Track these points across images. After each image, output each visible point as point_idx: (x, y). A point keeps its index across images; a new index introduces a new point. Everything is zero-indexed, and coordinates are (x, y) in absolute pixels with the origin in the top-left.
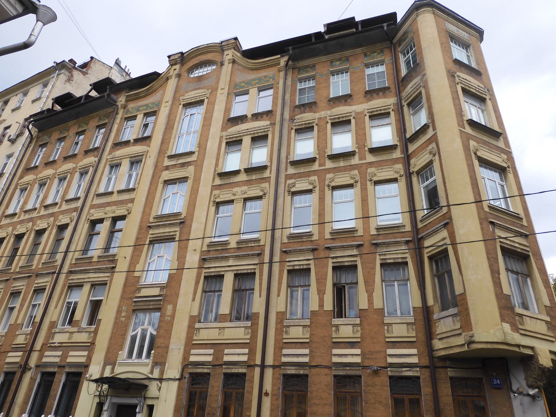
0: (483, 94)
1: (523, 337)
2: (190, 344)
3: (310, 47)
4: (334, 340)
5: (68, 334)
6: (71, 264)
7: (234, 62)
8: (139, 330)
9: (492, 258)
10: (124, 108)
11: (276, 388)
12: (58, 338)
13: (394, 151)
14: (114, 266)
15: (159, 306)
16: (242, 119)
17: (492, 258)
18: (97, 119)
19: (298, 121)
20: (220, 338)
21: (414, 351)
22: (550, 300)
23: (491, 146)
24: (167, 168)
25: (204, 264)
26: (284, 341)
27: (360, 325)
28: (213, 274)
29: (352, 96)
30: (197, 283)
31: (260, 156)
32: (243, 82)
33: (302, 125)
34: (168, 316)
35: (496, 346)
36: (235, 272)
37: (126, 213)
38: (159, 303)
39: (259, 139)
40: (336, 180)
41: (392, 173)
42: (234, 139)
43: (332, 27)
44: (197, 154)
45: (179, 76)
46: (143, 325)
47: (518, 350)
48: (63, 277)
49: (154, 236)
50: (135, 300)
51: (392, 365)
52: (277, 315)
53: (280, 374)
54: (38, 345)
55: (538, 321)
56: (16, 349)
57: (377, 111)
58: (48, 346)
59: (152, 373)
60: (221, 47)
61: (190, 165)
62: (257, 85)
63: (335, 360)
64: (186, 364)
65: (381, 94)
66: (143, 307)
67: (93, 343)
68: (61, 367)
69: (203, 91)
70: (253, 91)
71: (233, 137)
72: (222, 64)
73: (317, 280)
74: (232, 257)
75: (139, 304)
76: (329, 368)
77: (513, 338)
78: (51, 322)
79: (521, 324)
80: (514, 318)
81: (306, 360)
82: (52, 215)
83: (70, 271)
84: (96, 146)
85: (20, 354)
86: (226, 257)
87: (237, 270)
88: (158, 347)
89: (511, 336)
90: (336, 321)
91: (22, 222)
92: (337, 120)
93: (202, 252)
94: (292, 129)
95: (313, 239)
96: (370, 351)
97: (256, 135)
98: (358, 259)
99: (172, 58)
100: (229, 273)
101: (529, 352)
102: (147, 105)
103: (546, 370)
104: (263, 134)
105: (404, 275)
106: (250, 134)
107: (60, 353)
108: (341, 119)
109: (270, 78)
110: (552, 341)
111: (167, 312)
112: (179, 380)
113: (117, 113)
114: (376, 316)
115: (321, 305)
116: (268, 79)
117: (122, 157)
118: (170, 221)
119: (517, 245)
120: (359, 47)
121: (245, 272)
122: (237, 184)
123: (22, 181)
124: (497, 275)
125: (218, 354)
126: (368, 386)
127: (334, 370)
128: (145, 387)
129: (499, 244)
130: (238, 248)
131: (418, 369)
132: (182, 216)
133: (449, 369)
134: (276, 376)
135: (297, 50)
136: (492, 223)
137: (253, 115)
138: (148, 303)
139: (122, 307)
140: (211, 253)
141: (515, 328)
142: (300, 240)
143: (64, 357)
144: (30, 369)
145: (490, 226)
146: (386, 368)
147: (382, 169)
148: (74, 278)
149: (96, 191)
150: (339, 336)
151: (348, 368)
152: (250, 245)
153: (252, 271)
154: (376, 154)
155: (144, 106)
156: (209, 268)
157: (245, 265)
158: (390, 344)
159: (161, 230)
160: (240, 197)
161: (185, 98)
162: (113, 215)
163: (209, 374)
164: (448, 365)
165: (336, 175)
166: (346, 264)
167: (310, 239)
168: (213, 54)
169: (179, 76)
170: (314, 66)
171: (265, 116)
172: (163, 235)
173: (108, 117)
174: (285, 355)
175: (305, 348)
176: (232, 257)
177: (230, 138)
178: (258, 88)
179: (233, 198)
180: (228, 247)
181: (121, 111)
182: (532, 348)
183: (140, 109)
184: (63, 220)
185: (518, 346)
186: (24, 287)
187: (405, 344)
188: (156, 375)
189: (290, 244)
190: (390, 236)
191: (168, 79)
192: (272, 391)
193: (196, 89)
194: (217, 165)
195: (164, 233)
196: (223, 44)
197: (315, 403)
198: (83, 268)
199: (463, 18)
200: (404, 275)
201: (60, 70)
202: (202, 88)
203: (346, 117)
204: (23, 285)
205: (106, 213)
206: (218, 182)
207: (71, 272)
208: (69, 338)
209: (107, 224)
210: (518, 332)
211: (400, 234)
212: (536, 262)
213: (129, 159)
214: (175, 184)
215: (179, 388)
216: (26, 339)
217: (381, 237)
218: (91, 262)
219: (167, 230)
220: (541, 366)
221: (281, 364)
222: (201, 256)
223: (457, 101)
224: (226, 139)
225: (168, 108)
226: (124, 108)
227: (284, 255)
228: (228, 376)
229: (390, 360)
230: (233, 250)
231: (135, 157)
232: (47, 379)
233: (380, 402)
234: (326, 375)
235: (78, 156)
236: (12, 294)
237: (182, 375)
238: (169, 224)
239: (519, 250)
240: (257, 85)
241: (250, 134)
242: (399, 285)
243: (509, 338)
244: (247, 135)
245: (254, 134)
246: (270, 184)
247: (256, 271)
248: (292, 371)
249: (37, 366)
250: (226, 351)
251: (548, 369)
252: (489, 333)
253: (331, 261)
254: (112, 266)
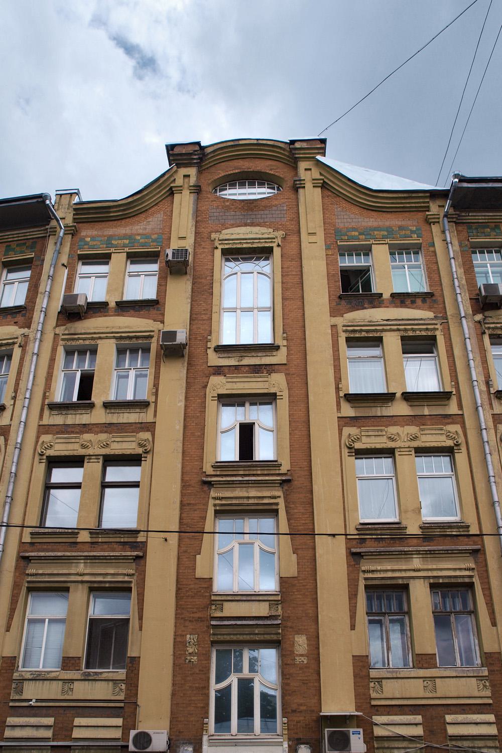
4: (374, 703)
8: (233, 680)
13: (390, 404)
14: (141, 554)
16: (97, 308)
21: (491, 718)
24: (219, 371)
25: (26, 568)
28: (107, 585)
30: (353, 596)
31: (422, 375)
32: (354, 229)
34: (302, 655)
38: (273, 630)
39: (418, 344)
41: (443, 438)
42: (364, 334)
44: (284, 350)
46: (239, 670)
49: (224, 502)
61: (274, 371)
62: (388, 241)
66: (228, 638)
69: (264, 230)
70: (118, 258)
71: (361, 331)
72: (297, 187)
74: (86, 558)
75: (218, 631)
86: (406, 553)
88: (294, 711)
94: (484, 333)
97: (411, 334)
98: (475, 573)
100: (417, 581)
102: (129, 237)
104: (424, 333)
105: (465, 604)
106: (398, 330)
109: (412, 232)
111: (297, 647)
116: (408, 232)
118: (254, 475)
122: (393, 420)
125: (63, 729)
130: (92, 543)
132: (283, 469)
137: (393, 295)
138: (247, 630)
139: (184, 636)
149: (45, 397)
150: (383, 696)
154: (357, 405)
155: (125, 237)
157: (451, 568)
159: (239, 492)
160: (407, 444)
161: (222, 237)
168: (270, 162)
169: (197, 190)
171: (419, 301)
172: (245, 501)
173: (32, 247)
174: (47, 727)
175: (118, 717)
176: (418, 552)
178: (128, 253)
179: (82, 452)
183: (386, 233)
191: (171, 193)
194: (338, 379)
195: (248, 498)
196: (297, 145)
198: (59, 554)
200: (465, 604)
202: (258, 225)
203: (376, 331)
206: (348, 411)
213: (113, 341)
214: (243, 405)
218: (76, 543)
219: (253, 493)
222: (19, 552)
230: (415, 541)
231: (130, 338)
238: (256, 482)
240: (127, 250)
241: (398, 330)
244: (107, 338)
245: (406, 330)
246: (6, 440)
247: (474, 580)
250: (78, 721)
253: (362, 575)
254: (135, 553)
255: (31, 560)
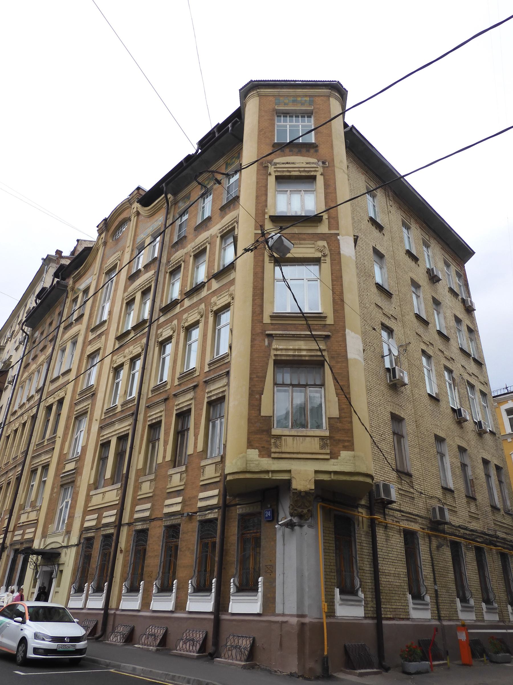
0: (311, 171)
1: (276, 461)
2: (86, 512)
3: (180, 176)
5: (179, 475)
6: (148, 399)
7: (138, 214)
10: (73, 290)
11: (129, 544)
12: (24, 518)
15: (72, 480)
17: (257, 377)
18: (59, 307)
19: (172, 262)
20: (103, 502)
23: (304, 236)
26: (138, 498)
27: (186, 471)
29: (317, 146)
33: (174, 265)
36: (118, 436)
37: (229, 300)
40: (189, 319)
43: (202, 143)
45: (105, 243)
47: (267, 477)
48: (141, 417)
50: (61, 476)
51: (202, 509)
53: (132, 531)
54: (11, 528)
56: (206, 487)
57: (226, 228)
58: (136, 502)
59: (63, 542)
60: (129, 202)
63: (166, 510)
64: (84, 530)
65: (232, 206)
67: (37, 520)
68: (22, 543)
73: (165, 430)
76: (160, 519)
77: (259, 464)
78: (20, 505)
79: (276, 447)
80: (269, 442)
81: (147, 514)
82: (201, 301)
83: (101, 427)
84: (206, 216)
85: (216, 492)
87: (119, 433)
89: (257, 463)
90: (171, 471)
91: (22, 414)
92: (198, 251)
93: (101, 420)
95: (167, 389)
96: (189, 498)
97: (144, 288)
99: (100, 227)
101: (285, 477)
107: (149, 506)
108: (201, 249)
112: (77, 545)
113: (67, 297)
114: (197, 460)
115: (164, 457)
117: (66, 342)
120: (219, 159)
121: (123, 434)
123: (23, 379)
124: (257, 396)
126: (184, 533)
127: (165, 521)
128: (59, 554)
129: (274, 358)
131: (217, 510)
132: (197, 373)
133: (238, 506)
134: (130, 533)
135: (171, 184)
136: (270, 336)
140: (107, 420)
142: (159, 392)
143: (99, 519)
144: (7, 548)
146: (196, 513)
147: (221, 295)
148: (212, 389)
151: (172, 518)
152: (129, 406)
153: (220, 395)
156: (103, 436)
158: (203, 487)
162: (131, 356)
163: (93, 537)
164: (237, 502)
165: (189, 314)
166: (185, 409)
167: (165, 389)
170: (190, 193)
177: (143, 287)
180: (116, 412)
181: (70, 294)
182: (289, 471)
184: (118, 361)
185: (267, 472)
186: (163, 413)
187: (212, 485)
188: (64, 544)
189: (153, 398)
190: (218, 369)
192: (126, 549)
193: (114, 253)
197: (149, 556)
199: (303, 81)
201: (48, 265)
204: (161, 412)
205: (125, 357)
207: (33, 458)
208: (28, 518)
209: (126, 367)
210: (269, 456)
211: (225, 366)
215: (77, 553)
216: (181, 480)
217: (211, 372)
220: (295, 491)
221: (163, 516)
223: (263, 198)
224: (126, 300)
225: (96, 281)
226: (73, 290)
227: (148, 409)
228: (204, 523)
229: (200, 504)
232: (141, 536)
233: (189, 548)
234: (159, 527)
235: (213, 219)
236: (210, 403)
237: (80, 541)
239: (307, 358)
243: (252, 465)
248: (139, 526)
249: (11, 545)
251: (307, 493)
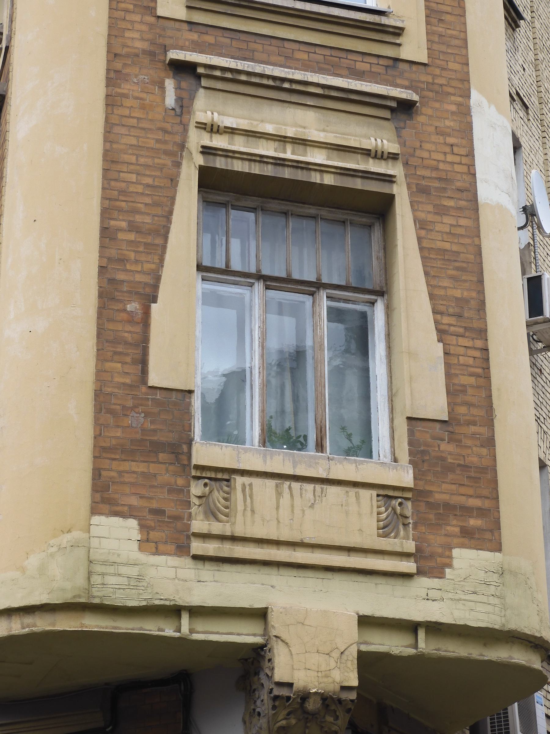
1: (208, 572)
9: (133, 227)
17: (133, 227)
22: (453, 391)
35: (42, 624)
47: (169, 632)
52: (491, 515)
55: (333, 490)
79: (212, 513)
80: (184, 491)
101: (245, 634)
103: (312, 705)
110: (406, 576)
119: (318, 157)
124: (133, 306)
129: (200, 160)
136: (183, 69)
141: (168, 532)
145: (170, 84)
182: (261, 615)
210: (182, 549)
212: (421, 225)
220: (284, 692)
239: (329, 180)
242: (266, 307)
243: (112, 580)
251: (327, 701)
252: (23, 570)
255: (199, 77)
